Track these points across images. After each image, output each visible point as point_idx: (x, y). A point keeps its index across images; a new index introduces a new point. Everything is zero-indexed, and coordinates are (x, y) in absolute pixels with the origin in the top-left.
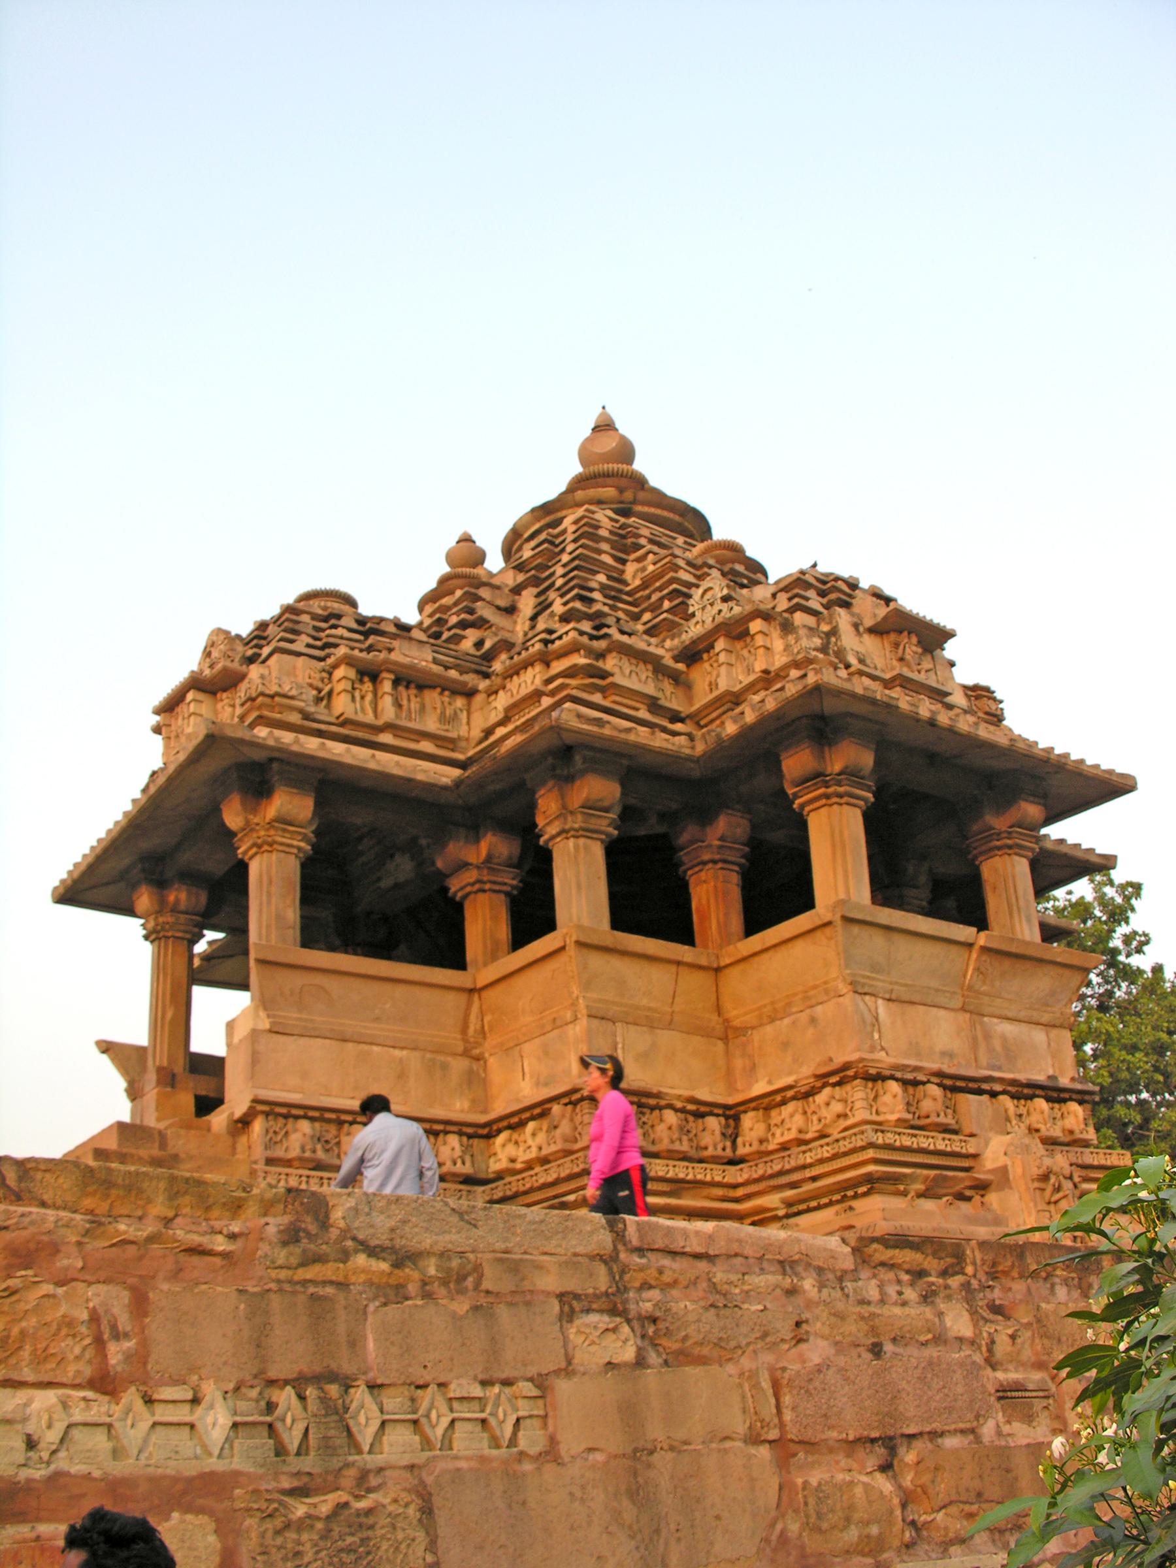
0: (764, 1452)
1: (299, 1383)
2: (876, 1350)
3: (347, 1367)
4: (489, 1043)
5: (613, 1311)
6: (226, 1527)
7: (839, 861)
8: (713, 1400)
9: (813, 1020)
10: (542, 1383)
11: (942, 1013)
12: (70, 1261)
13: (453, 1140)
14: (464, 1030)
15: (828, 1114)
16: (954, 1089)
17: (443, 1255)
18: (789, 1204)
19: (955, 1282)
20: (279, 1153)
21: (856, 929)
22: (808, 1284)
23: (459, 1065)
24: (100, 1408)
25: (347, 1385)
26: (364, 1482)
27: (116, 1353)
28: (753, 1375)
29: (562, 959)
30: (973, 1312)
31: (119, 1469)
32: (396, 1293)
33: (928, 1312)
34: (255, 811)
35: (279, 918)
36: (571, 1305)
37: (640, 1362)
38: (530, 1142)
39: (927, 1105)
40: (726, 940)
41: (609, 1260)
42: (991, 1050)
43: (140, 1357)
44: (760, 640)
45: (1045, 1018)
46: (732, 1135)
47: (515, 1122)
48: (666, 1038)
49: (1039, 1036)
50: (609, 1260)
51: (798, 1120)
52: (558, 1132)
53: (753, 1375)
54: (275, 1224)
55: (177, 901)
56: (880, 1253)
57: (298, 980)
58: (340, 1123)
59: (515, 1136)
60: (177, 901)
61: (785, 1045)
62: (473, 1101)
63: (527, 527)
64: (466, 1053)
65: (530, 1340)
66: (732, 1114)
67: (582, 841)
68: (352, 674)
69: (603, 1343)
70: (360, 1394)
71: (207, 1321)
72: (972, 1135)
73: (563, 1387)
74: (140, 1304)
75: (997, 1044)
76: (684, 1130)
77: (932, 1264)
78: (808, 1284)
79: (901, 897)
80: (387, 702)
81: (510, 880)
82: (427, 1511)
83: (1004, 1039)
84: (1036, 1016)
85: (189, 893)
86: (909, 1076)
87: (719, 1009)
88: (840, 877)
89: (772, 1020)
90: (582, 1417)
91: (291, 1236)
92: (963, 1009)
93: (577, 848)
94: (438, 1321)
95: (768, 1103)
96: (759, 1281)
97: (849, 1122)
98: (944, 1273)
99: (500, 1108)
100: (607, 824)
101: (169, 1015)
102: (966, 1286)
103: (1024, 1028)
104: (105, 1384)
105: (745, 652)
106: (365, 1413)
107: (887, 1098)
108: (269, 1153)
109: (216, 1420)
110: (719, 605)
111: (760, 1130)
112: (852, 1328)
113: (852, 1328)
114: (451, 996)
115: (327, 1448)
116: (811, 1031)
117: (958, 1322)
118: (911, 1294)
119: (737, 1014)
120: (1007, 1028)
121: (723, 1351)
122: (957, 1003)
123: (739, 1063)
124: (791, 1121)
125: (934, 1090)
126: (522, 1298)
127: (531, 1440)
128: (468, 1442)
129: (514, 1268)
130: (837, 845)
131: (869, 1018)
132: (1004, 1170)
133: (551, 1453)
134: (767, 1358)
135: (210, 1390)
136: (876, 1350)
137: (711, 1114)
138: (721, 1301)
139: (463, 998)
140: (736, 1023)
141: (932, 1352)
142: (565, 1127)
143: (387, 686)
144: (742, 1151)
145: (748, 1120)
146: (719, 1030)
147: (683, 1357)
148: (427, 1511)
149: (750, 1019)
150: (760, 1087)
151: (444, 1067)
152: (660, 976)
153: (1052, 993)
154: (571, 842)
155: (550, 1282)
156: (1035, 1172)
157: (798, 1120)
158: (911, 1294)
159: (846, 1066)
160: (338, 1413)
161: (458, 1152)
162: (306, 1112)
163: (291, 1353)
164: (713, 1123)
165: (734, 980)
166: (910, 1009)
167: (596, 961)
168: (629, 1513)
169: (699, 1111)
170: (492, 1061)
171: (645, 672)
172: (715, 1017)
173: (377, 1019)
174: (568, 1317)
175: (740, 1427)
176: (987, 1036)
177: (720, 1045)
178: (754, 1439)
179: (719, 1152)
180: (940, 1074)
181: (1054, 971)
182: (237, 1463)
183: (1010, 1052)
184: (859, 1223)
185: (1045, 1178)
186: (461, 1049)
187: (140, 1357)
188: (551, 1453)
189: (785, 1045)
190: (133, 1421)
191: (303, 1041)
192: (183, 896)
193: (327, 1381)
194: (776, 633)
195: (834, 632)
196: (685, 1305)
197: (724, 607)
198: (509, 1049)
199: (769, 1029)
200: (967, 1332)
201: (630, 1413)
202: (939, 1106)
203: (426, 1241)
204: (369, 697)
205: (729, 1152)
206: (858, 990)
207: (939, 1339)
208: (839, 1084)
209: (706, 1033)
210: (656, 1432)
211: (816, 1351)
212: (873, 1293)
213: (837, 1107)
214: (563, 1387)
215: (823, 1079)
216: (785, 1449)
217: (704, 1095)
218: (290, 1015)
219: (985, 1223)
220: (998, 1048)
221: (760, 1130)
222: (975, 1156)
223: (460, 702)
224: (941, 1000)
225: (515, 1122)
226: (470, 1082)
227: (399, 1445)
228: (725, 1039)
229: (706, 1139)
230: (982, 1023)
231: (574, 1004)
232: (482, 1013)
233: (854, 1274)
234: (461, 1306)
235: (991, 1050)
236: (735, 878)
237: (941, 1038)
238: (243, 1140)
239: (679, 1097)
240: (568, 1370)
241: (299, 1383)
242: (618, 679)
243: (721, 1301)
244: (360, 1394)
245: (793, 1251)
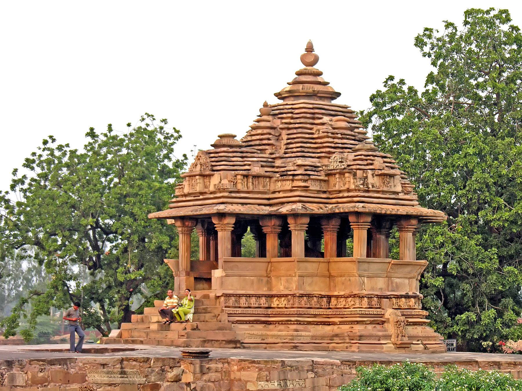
0: (327, 387)
1: (283, 380)
2: (342, 375)
4: (273, 274)
9: (350, 280)
10: (304, 379)
11: (381, 278)
12: (264, 370)
13: (264, 299)
14: (267, 271)
16: (380, 298)
18: (340, 322)
19: (354, 366)
20: (227, 305)
22: (335, 367)
23: (265, 279)
24: (267, 383)
25: (287, 380)
27: (268, 378)
28: (327, 379)
29: (293, 263)
32: (291, 371)
33: (350, 370)
34: (221, 221)
35: (227, 247)
36: (308, 371)
37: (315, 377)
38: (283, 302)
39: (373, 303)
42: (392, 286)
44: (347, 179)
45: (409, 276)
46: (329, 302)
47: (280, 296)
48: (315, 279)
49: (407, 281)
51: (344, 303)
53: (327, 379)
55: (188, 225)
57: (232, 264)
58: (240, 296)
60: (188, 225)
62: (268, 288)
63: (284, 94)
64: (267, 276)
65: (304, 375)
66: (329, 297)
68: (242, 177)
69: (311, 375)
71: (275, 374)
73: (307, 380)
74: (270, 373)
75: (394, 285)
76: (318, 302)
77: (351, 364)
78: (335, 367)
79: (380, 231)
80: (250, 184)
81: (279, 230)
83: (396, 283)
87: (328, 270)
90: (308, 383)
91: (282, 365)
95: (337, 297)
96: (329, 367)
99: (274, 293)
100: (305, 227)
104: (267, 381)
105: (343, 179)
109: (276, 384)
110: (338, 163)
111: (335, 302)
112: (340, 373)
114: (264, 263)
115: (285, 386)
117: (354, 371)
118: (348, 368)
119: (333, 273)
121: (324, 376)
123: (332, 284)
124: (342, 303)
125: (375, 299)
126: (303, 371)
127: (303, 386)
128: (298, 386)
130: (360, 239)
131: (362, 282)
135: (276, 381)
136: (342, 375)
138: (324, 370)
139: (267, 264)
142: (291, 302)
143: (250, 180)
144: (331, 307)
145: (333, 299)
147: (320, 376)
150: (336, 293)
151: (262, 280)
152: (315, 265)
154: (297, 232)
155: (306, 369)
156: (395, 320)
157: (344, 303)
158: (348, 368)
159: (355, 295)
160: (286, 383)
164: (325, 300)
169: (322, 297)
170: (273, 278)
171: (317, 183)
172: (327, 272)
174: (308, 372)
175: (325, 384)
176: (392, 283)
178: (326, 386)
182: (278, 388)
183: (398, 287)
184: (354, 331)
185: (397, 322)
186: (265, 275)
187: (270, 378)
188: (305, 387)
190: (269, 384)
192: (190, 224)
193: (285, 380)
194: (352, 177)
196: (320, 370)
197: (340, 164)
198: (278, 277)
199: (340, 278)
201: (313, 383)
205: (328, 307)
206: (360, 276)
207: (351, 374)
209: (324, 276)
210: (316, 385)
211: (335, 375)
213: (353, 303)
214: (307, 380)
217: (323, 293)
218: (230, 272)
219: (383, 331)
221: (335, 302)
223: (268, 180)
225: (280, 296)
226: (267, 283)
227: (291, 386)
228: (329, 277)
229: (323, 304)
230: (391, 280)
231: (295, 273)
233: (340, 366)
235: (392, 286)
236: (336, 234)
237: (380, 285)
238: (218, 300)
240: (307, 378)
241: (283, 380)
242: (310, 188)
243: (324, 370)
245: (333, 363)
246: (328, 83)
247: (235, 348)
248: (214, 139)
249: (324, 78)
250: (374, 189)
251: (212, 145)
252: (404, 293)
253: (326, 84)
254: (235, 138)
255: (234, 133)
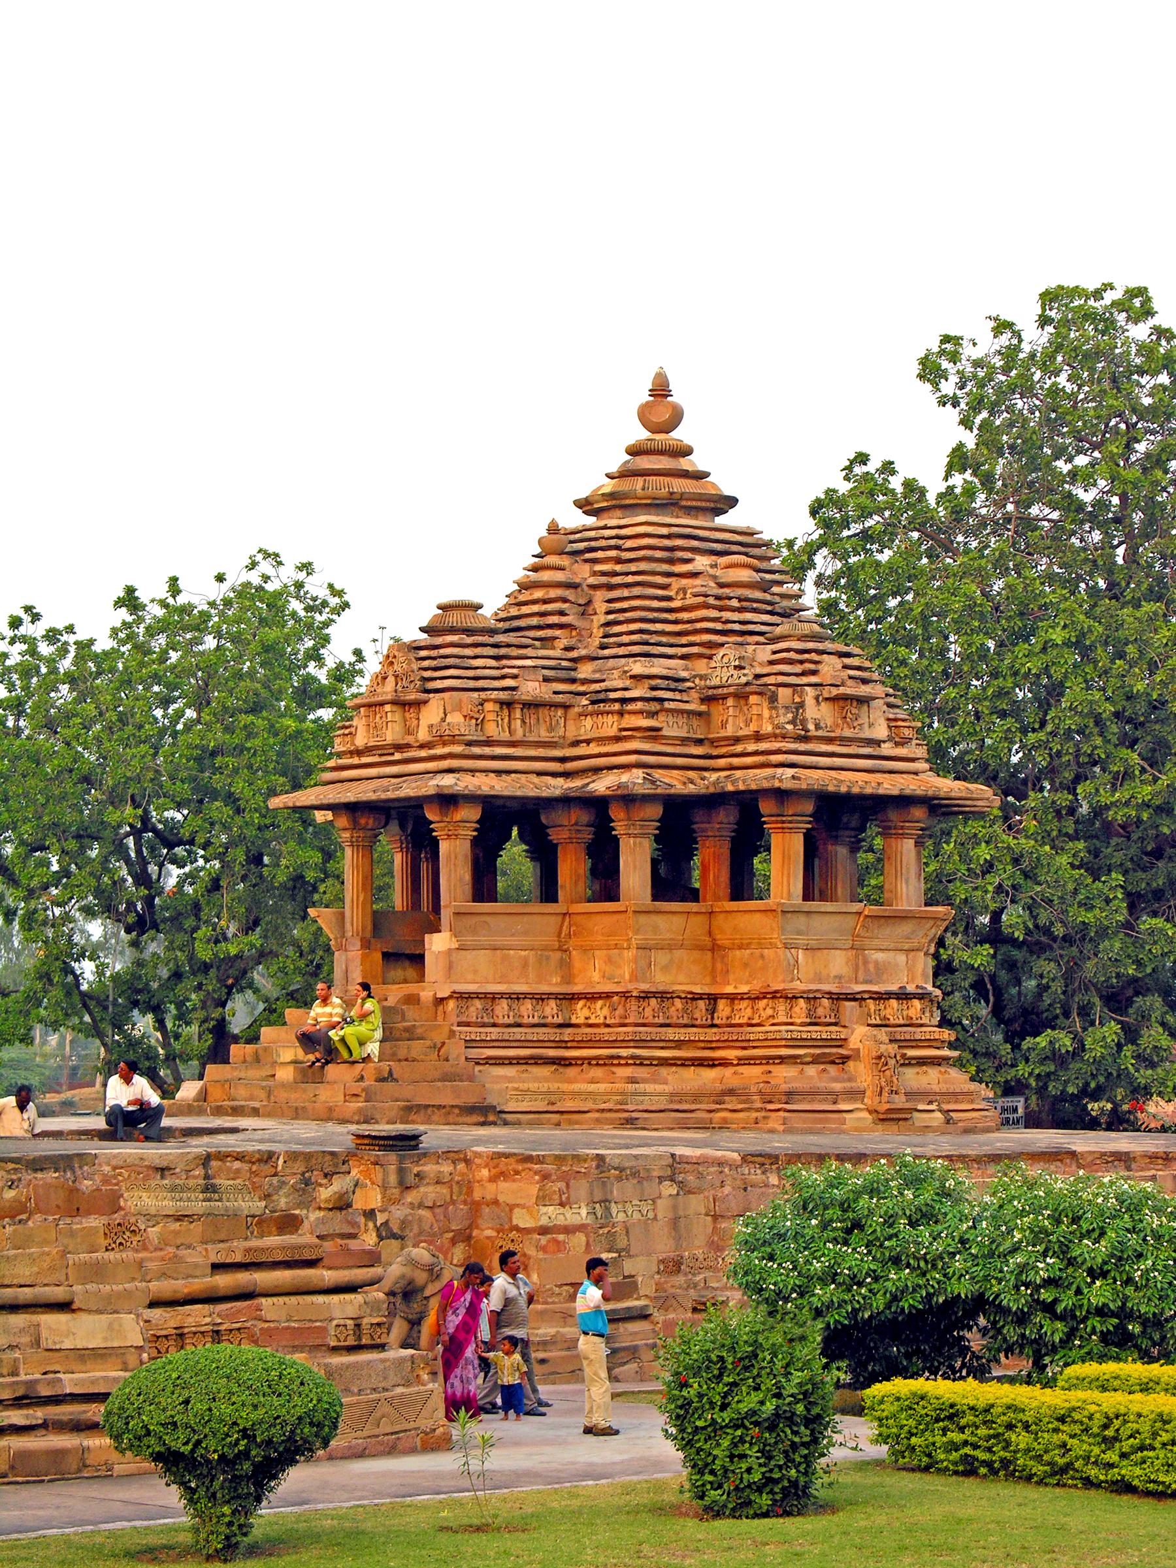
0: (709, 1218)
1: (600, 1202)
2: (745, 1189)
3: (609, 1198)
5: (672, 1180)
6: (587, 1236)
7: (786, 872)
8: (696, 1204)
9: (762, 956)
11: (838, 952)
12: (554, 1177)
13: (552, 1003)
14: (559, 935)
15: (764, 1015)
17: (631, 1168)
19: (774, 1167)
21: (789, 915)
24: (562, 1210)
26: (613, 1226)
30: (779, 1177)
31: (566, 1223)
32: (619, 1179)
33: (764, 1177)
36: (661, 1179)
37: (678, 1194)
39: (820, 1011)
40: (718, 899)
41: (671, 1166)
42: (866, 970)
43: (568, 1198)
44: (755, 710)
45: (906, 947)
47: (592, 997)
48: (678, 953)
49: (901, 958)
50: (671, 1166)
52: (617, 1012)
53: (707, 1197)
54: (594, 1164)
56: (750, 1158)
59: (588, 1004)
61: (746, 965)
64: (560, 949)
65: (651, 1188)
66: (713, 999)
67: (638, 840)
68: (497, 707)
69: (669, 1189)
70: (613, 1204)
71: (581, 1188)
72: (844, 1027)
73: (659, 1201)
74: (568, 1186)
77: (768, 1161)
81: (588, 835)
82: (627, 1232)
83: (876, 963)
84: (900, 946)
85: (375, 819)
86: (811, 996)
88: (785, 879)
89: (740, 948)
91: (598, 1167)
92: (852, 948)
93: (635, 843)
94: (630, 1185)
95: (732, 998)
96: (712, 1169)
97: (775, 1021)
98: (771, 1164)
99: (577, 988)
101: (361, 899)
102: (778, 1168)
103: (892, 954)
104: (562, 1204)
106: (614, 1209)
107: (797, 1009)
108: (459, 1019)
109: (584, 1212)
110: (732, 671)
113: (738, 1182)
116: (760, 962)
117: (773, 1180)
118: (758, 1171)
119: (722, 939)
120: (879, 956)
122: (849, 944)
123: (719, 966)
124: (744, 1012)
125: (825, 1002)
128: (637, 1216)
129: (648, 1170)
130: (786, 857)
131: (792, 962)
132: (858, 1050)
133: (655, 1218)
134: (712, 1192)
135: (582, 1205)
137: (701, 999)
138: (700, 1176)
140: (718, 942)
141: (764, 1189)
142: (620, 1011)
143: (518, 713)
144: (716, 1022)
145: (721, 1004)
146: (710, 945)
147: (690, 1192)
148: (627, 1232)
149: (727, 943)
150: (729, 989)
151: (548, 958)
152: (678, 921)
153: (914, 932)
154: (632, 840)
155: (656, 1174)
156: (874, 1054)
157: (749, 1012)
158: (758, 1171)
159: (776, 992)
160: (608, 1209)
161: (555, 1011)
162: (478, 996)
163: (598, 1196)
164: (701, 1004)
165: (720, 920)
166: (819, 953)
167: (643, 919)
168: (673, 1234)
173: (513, 935)
174: (660, 1183)
175: (703, 1211)
176: (866, 962)
177: (709, 953)
178: (707, 1215)
179: (704, 1022)
180: (829, 993)
181: (914, 921)
182: (588, 1221)
183: (881, 971)
185: (879, 1058)
187: (568, 1198)
188: (655, 1218)
189: (746, 965)
191: (474, 952)
193: (605, 1201)
195: (801, 705)
197: (735, 673)
199: (738, 952)
200: (776, 1183)
201: (675, 1208)
202: (828, 1012)
203: (627, 1165)
204: (506, 720)
207: (767, 1186)
208: (773, 998)
209: (701, 948)
210: (681, 1213)
211: (727, 1190)
212: (747, 1172)
213: (769, 1012)
214: (659, 1201)
215: (762, 996)
216: (715, 1217)
217: (698, 989)
219: (843, 1081)
220: (872, 969)
222: (845, 1040)
223: (560, 712)
224: (839, 946)
225: (592, 997)
227: (621, 1217)
228: (712, 950)
229: (697, 1015)
231: (629, 940)
232: (570, 925)
233: (741, 1166)
234: (635, 1181)
237: (836, 968)
239: (684, 992)
240: (660, 1197)
242: (664, 733)
243: (700, 1176)
244: (613, 1204)
246: (707, 475)
247: (483, 1124)
248: (427, 614)
249: (698, 461)
250: (820, 733)
251: (422, 629)
252: (894, 988)
253: (701, 476)
254: (480, 611)
255: (476, 600)
